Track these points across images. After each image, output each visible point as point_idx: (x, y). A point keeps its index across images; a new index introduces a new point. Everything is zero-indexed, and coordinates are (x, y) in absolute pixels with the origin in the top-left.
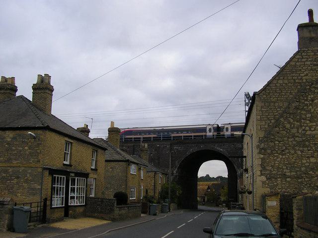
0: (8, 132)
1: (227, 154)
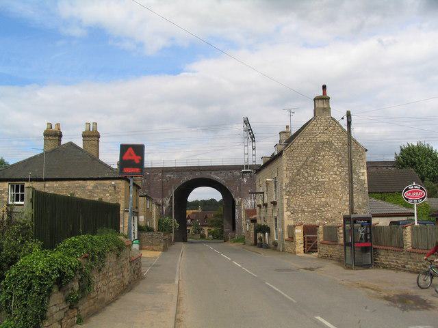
0: (89, 182)
1: (223, 182)
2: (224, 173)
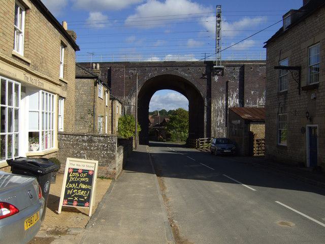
2: (192, 69)
